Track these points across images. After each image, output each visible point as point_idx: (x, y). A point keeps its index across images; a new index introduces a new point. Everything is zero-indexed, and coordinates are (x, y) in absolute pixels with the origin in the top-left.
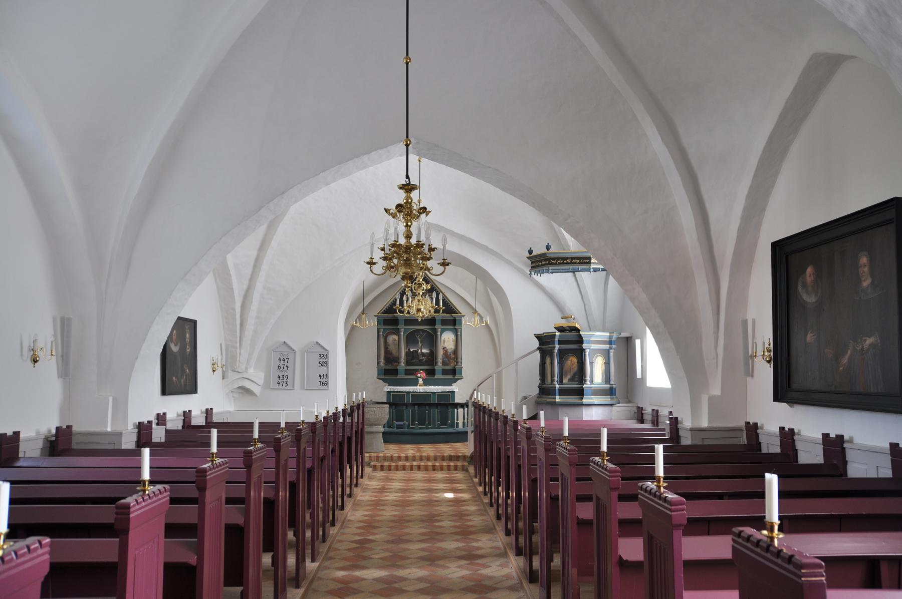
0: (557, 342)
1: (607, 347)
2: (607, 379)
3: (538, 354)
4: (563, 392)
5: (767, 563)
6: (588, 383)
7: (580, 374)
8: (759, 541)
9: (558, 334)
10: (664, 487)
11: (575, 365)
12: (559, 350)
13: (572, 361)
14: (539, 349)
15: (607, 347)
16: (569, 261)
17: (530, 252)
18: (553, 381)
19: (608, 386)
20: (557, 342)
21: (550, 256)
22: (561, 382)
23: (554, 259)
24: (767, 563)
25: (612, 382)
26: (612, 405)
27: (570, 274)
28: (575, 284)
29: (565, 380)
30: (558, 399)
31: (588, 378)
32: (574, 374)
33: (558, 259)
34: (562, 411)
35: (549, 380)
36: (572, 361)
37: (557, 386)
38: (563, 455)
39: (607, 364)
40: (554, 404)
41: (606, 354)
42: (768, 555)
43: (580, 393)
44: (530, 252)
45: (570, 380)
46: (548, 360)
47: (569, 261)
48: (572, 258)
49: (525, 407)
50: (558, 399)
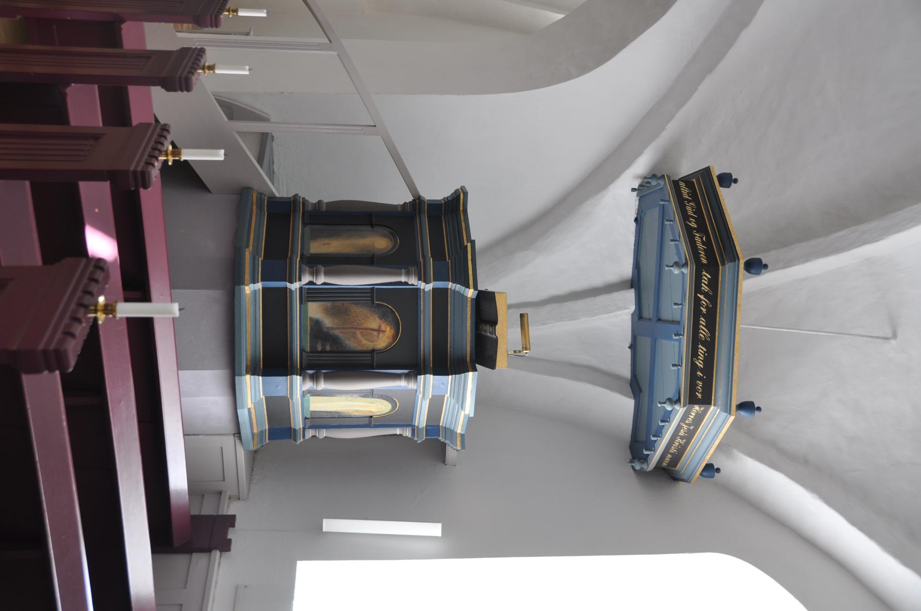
0: (440, 284)
1: (421, 420)
2: (317, 421)
3: (399, 196)
4: (276, 306)
5: (136, 159)
6: (309, 385)
7: (338, 361)
8: (162, 144)
9: (470, 293)
10: (166, 161)
11: (366, 344)
12: (416, 291)
13: (380, 335)
14: (418, 202)
15: (421, 420)
16: (704, 333)
17: (727, 180)
18: (315, 263)
19: (298, 423)
20: (440, 284)
21: (726, 271)
22: (311, 294)
23: (714, 283)
24: (143, 145)
25: (310, 433)
26: (238, 433)
27: (626, 269)
28: (598, 280)
29: (315, 310)
30: (252, 289)
31: (322, 386)
32: (335, 340)
33: (713, 298)
34: (208, 301)
35: (318, 247)
36: (380, 335)
37: (295, 286)
38: (101, 227)
39: (369, 421)
40: (234, 279)
41: (402, 416)
42: (66, 320)
43: (275, 362)
44: (727, 180)
45: (316, 324)
46: (380, 243)
47: (704, 333)
48: (710, 345)
49: (219, 155)
50: (252, 289)
